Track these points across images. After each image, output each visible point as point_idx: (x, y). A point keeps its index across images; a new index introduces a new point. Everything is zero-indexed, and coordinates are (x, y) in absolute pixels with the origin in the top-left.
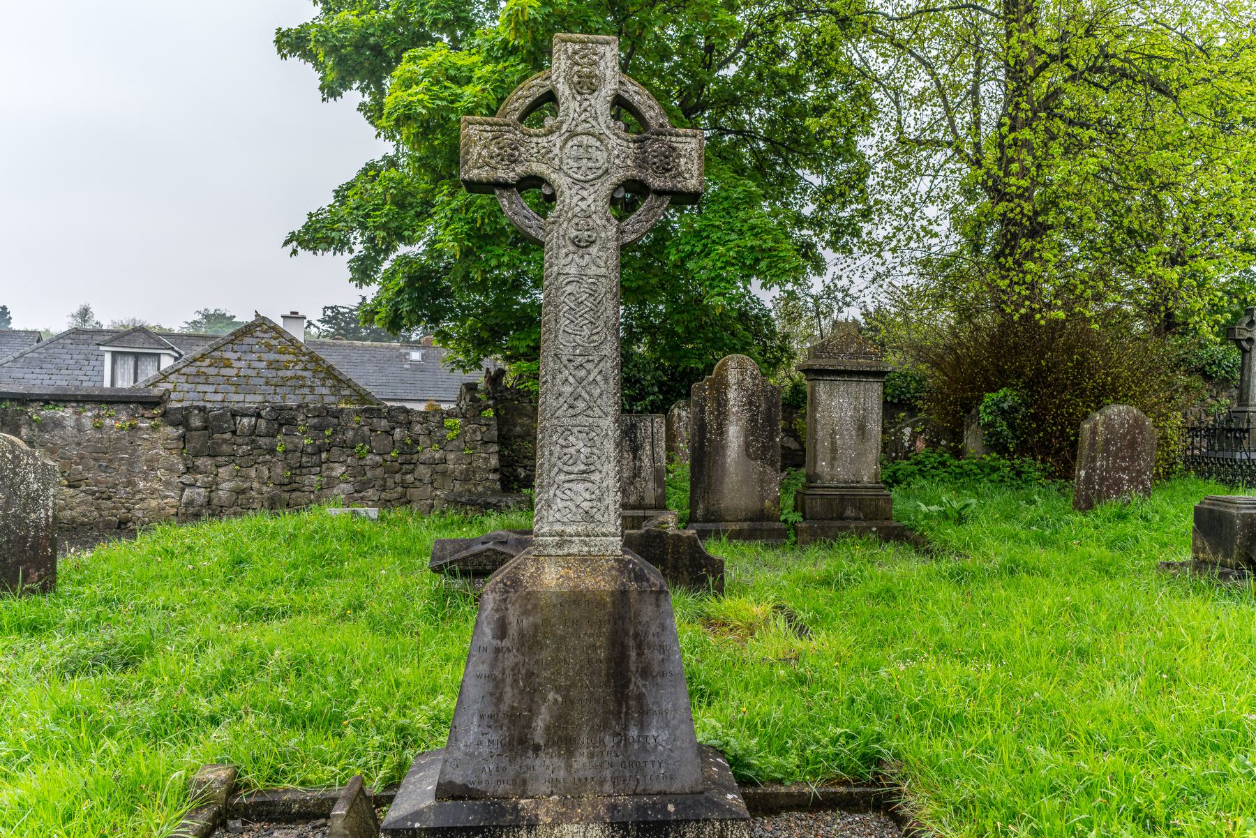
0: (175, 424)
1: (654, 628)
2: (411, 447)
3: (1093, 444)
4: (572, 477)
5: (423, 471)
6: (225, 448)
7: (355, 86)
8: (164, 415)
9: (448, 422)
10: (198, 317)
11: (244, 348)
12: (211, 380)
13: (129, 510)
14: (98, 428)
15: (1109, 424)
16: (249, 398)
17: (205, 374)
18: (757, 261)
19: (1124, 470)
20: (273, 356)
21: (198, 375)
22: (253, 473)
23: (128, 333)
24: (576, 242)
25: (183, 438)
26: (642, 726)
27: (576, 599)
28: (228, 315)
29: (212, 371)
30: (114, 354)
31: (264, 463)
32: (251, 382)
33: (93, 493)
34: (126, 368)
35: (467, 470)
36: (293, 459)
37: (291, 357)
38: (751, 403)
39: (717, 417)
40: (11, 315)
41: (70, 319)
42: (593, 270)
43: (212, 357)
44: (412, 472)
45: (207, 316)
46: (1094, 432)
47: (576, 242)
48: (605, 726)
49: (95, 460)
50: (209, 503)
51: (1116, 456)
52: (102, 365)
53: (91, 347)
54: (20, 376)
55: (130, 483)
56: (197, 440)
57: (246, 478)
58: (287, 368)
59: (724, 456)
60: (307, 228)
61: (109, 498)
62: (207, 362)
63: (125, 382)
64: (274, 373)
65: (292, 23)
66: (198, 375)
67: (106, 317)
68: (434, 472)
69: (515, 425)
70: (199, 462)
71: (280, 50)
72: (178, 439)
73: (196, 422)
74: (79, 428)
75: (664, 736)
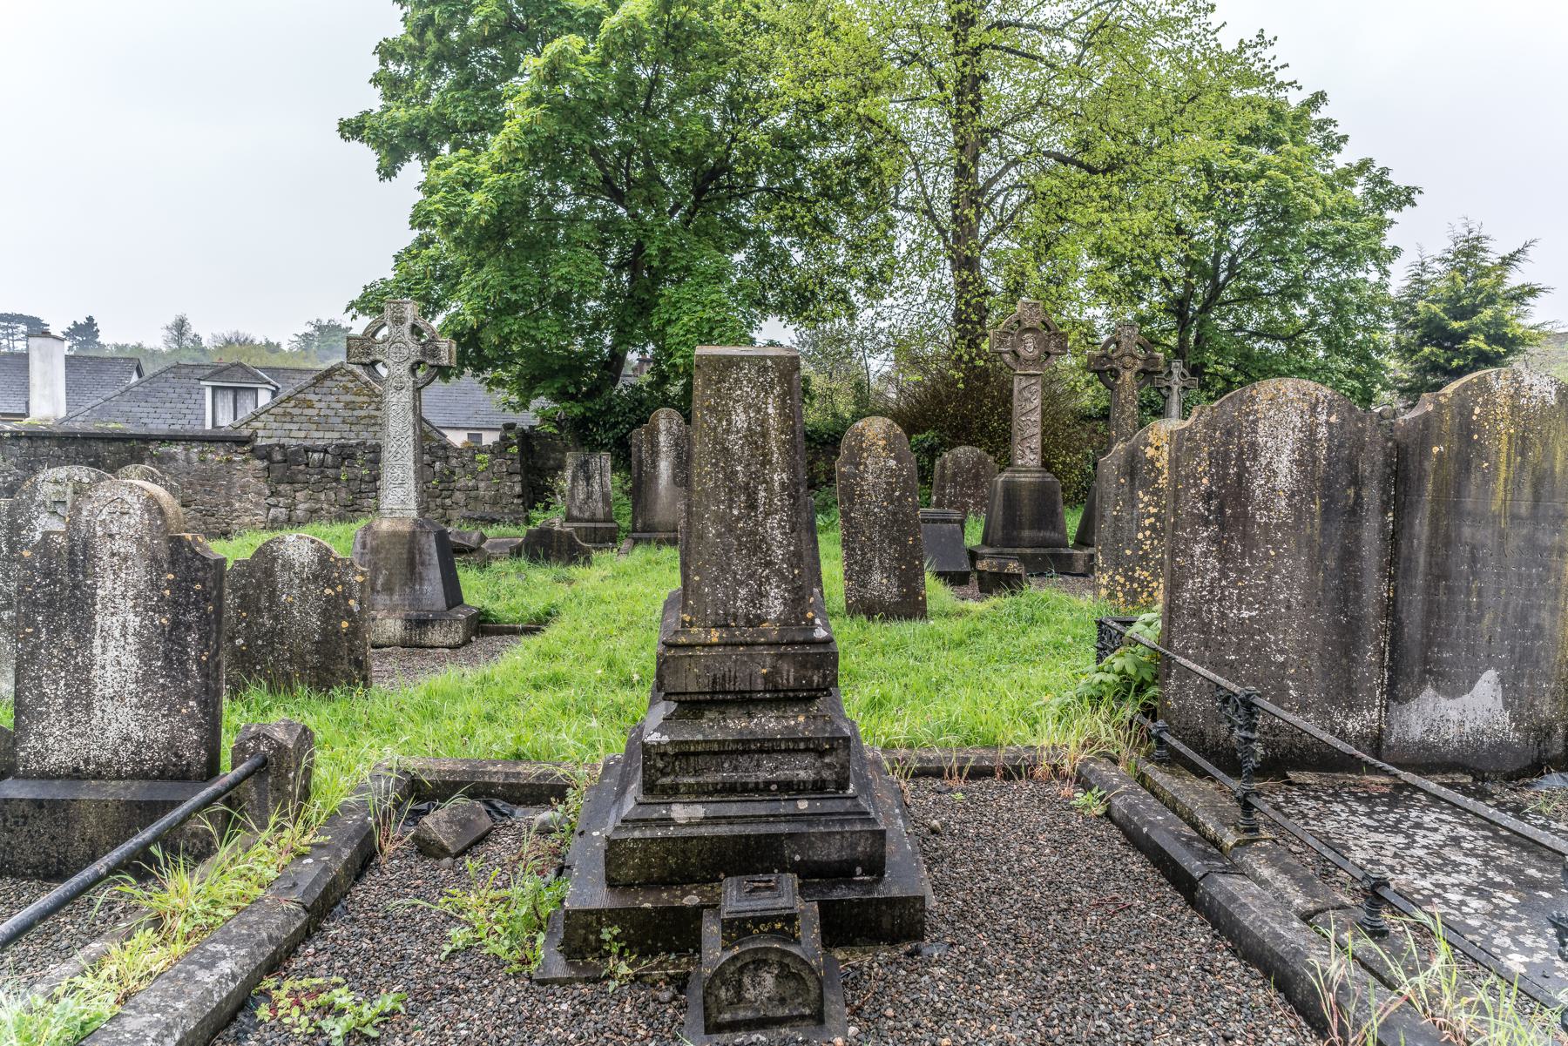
0: (261, 458)
1: (426, 546)
2: (449, 477)
3: (943, 476)
4: (1375, 589)
5: (458, 496)
6: (300, 477)
7: (414, 156)
8: (252, 451)
9: (478, 457)
10: (310, 329)
11: (325, 390)
12: (295, 419)
13: (228, 524)
14: (203, 461)
15: (956, 461)
16: (328, 435)
17: (290, 414)
18: (712, 329)
19: (970, 496)
20: (349, 398)
21: (284, 415)
22: (323, 497)
23: (226, 369)
24: (396, 388)
25: (268, 469)
26: (421, 585)
27: (394, 534)
28: (343, 326)
29: (297, 411)
30: (214, 389)
31: (331, 489)
32: (331, 420)
33: (201, 512)
34: (226, 402)
35: (495, 496)
36: (354, 486)
37: (365, 399)
38: (677, 445)
39: (651, 455)
40: (99, 327)
41: (165, 332)
42: (404, 400)
43: (297, 399)
44: (450, 497)
45: (320, 328)
46: (943, 467)
47: (396, 388)
48: (406, 584)
49: (202, 485)
50: (289, 519)
51: (962, 486)
52: (204, 399)
53: (193, 381)
54: (127, 409)
55: (229, 504)
56: (278, 470)
57: (318, 501)
58: (361, 408)
59: (657, 484)
60: (363, 297)
61: (213, 515)
62: (293, 403)
63: (225, 420)
64: (350, 413)
65: (352, 114)
66: (284, 415)
67: (209, 330)
68: (468, 497)
69: (548, 459)
70: (281, 488)
71: (342, 136)
72: (264, 469)
73: (278, 457)
74: (188, 461)
75: (430, 589)
